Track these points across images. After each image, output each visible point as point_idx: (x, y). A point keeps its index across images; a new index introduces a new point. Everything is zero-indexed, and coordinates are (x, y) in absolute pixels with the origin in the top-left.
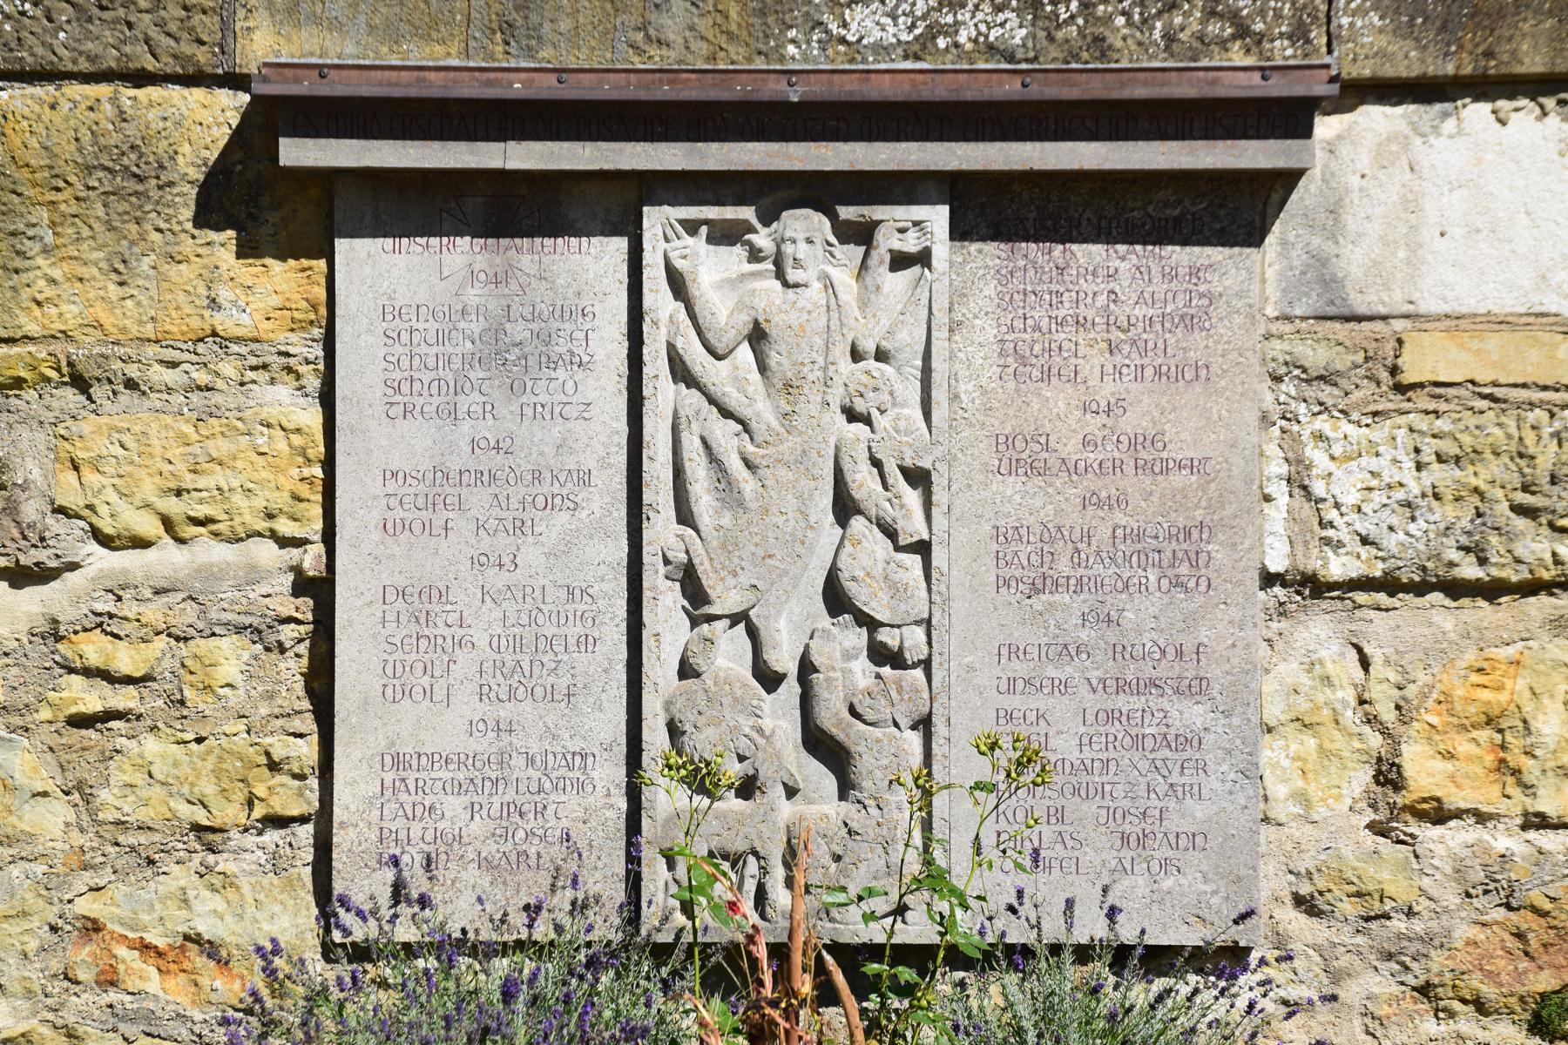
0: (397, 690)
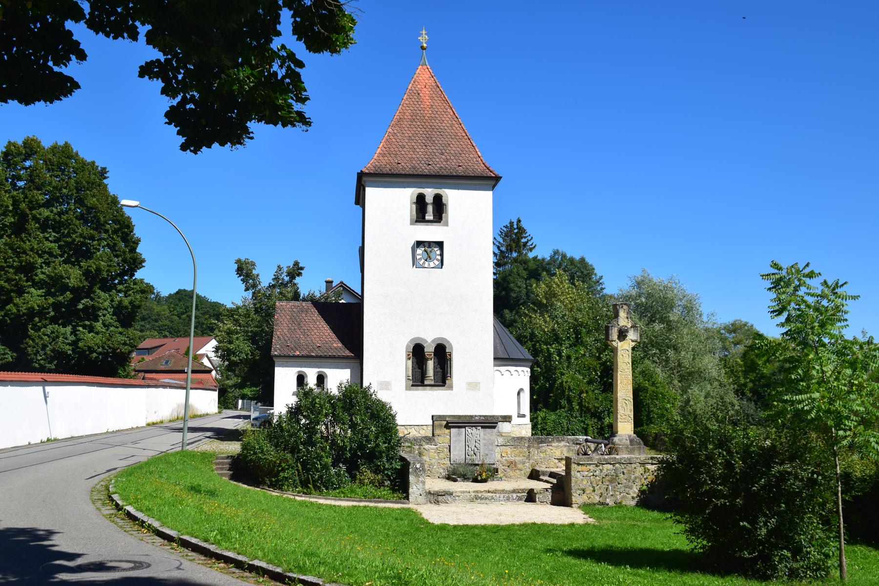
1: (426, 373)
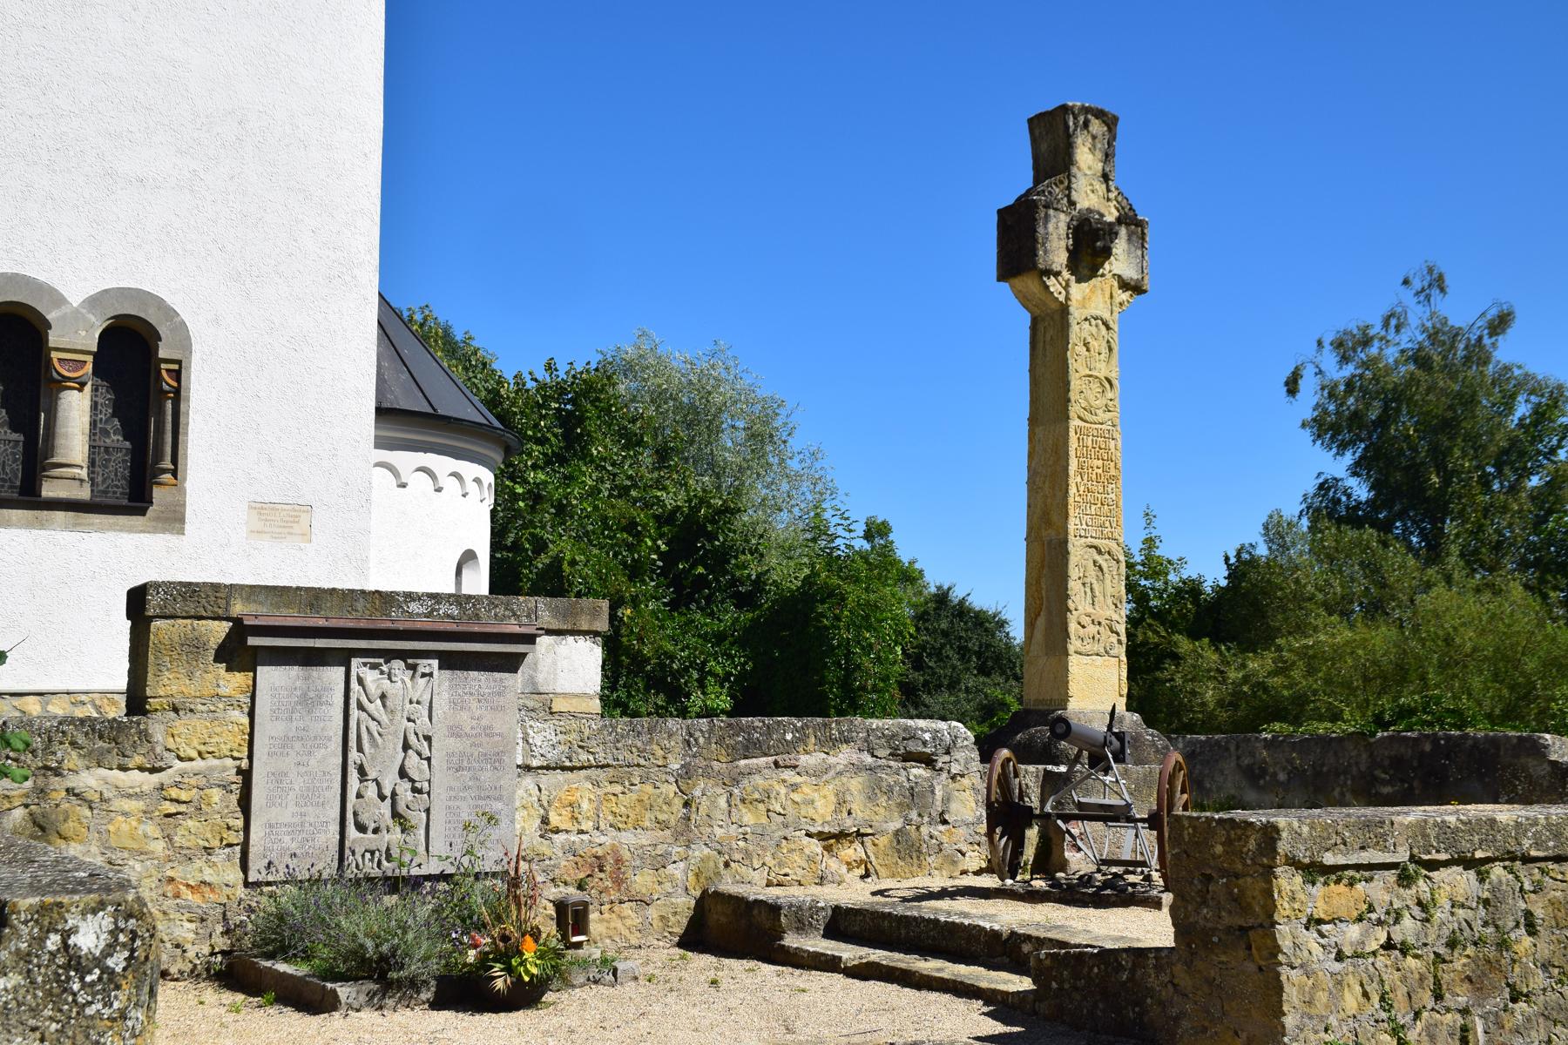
0: (271, 803)
1: (50, 448)
